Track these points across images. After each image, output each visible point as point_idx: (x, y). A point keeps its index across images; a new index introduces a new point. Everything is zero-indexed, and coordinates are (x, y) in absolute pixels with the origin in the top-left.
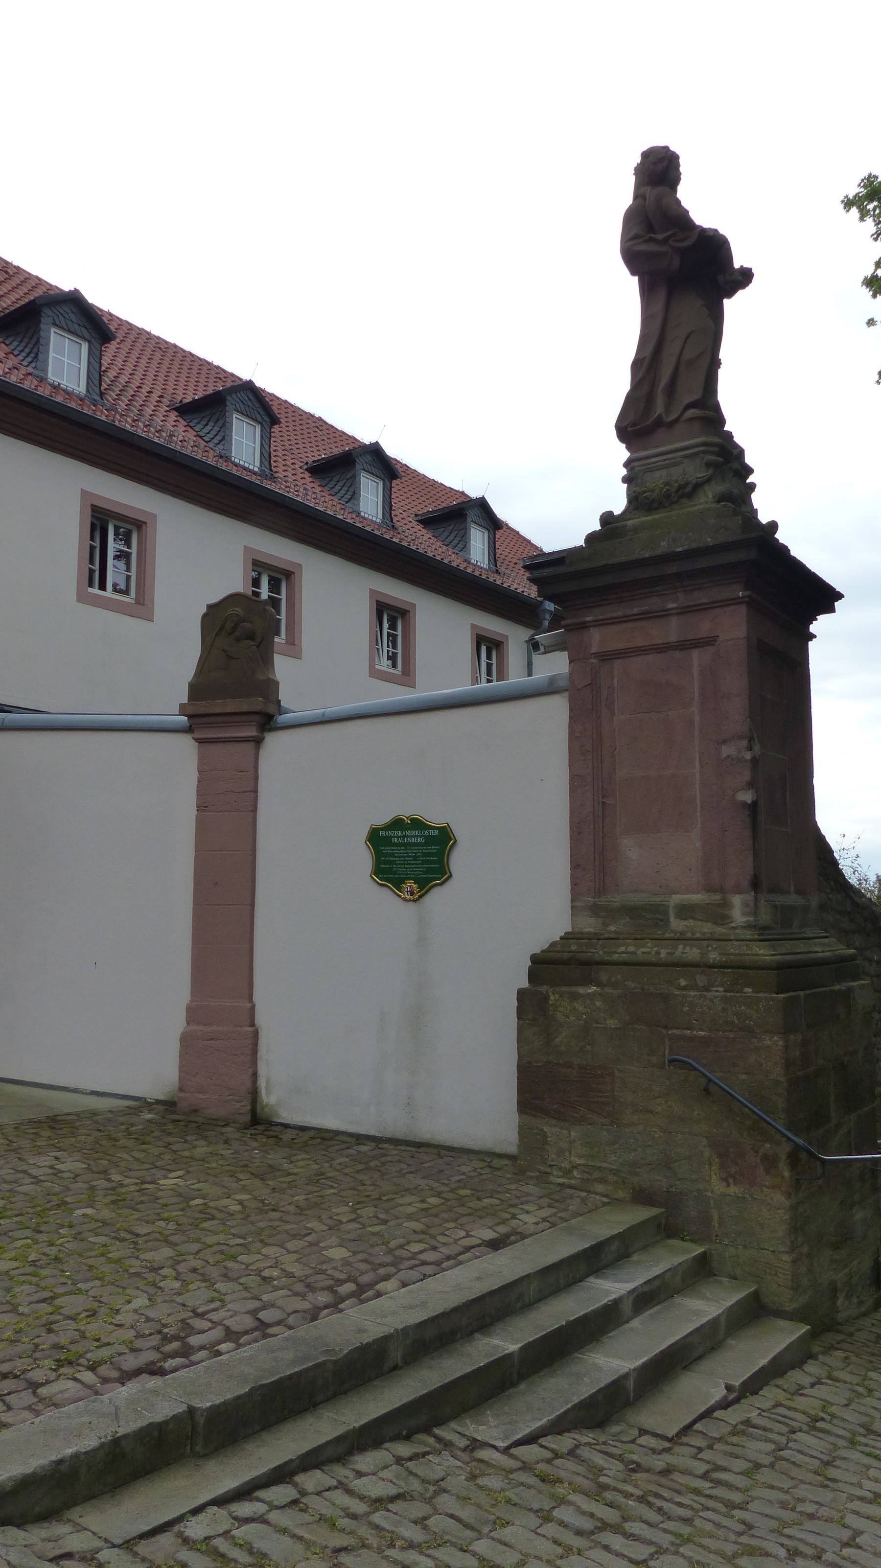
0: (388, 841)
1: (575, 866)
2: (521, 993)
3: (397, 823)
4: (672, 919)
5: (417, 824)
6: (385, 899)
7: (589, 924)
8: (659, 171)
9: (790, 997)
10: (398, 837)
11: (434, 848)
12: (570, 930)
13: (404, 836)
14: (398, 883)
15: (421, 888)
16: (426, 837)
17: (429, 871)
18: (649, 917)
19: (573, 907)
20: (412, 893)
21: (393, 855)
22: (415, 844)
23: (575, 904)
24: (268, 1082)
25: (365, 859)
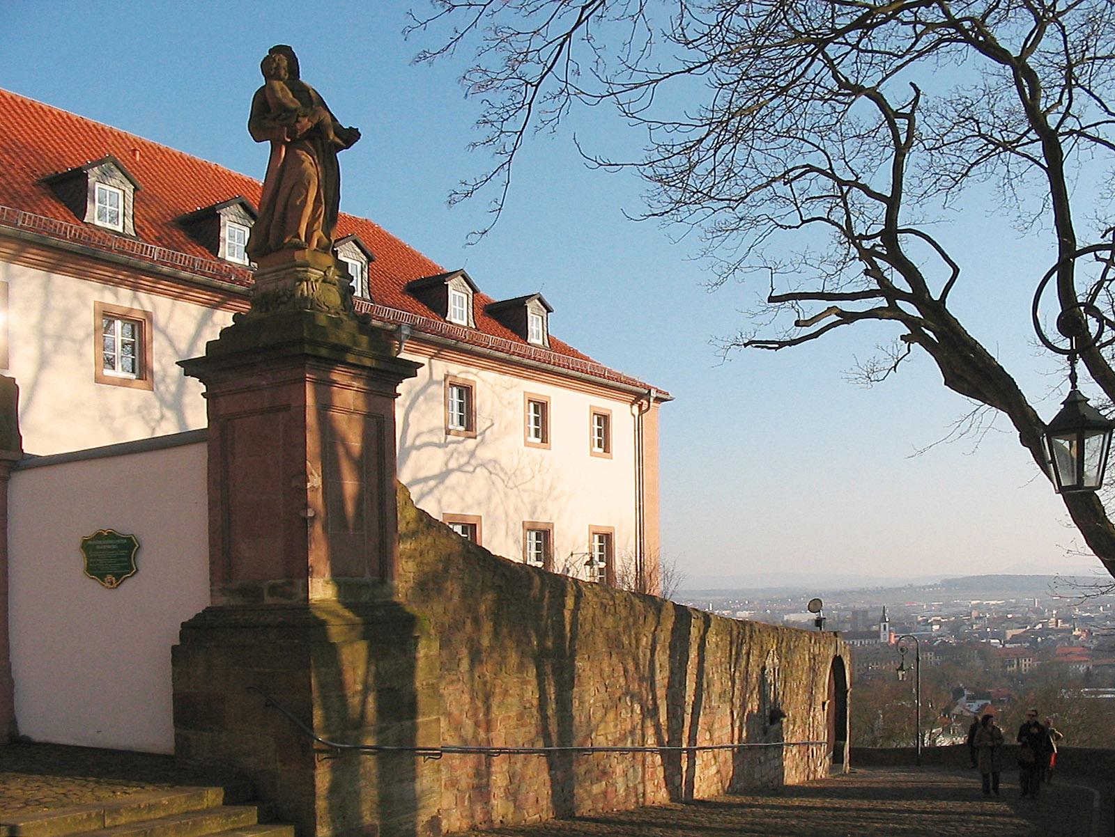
0: (94, 548)
1: (212, 563)
2: (174, 648)
3: (99, 536)
4: (266, 597)
5: (112, 535)
6: (93, 586)
7: (222, 601)
8: (281, 63)
9: (564, 627)
10: (100, 545)
11: (124, 553)
12: (209, 605)
13: (836, 825)
14: (102, 577)
15: (117, 580)
16: (118, 545)
17: (123, 568)
18: (251, 592)
19: (211, 590)
20: (112, 584)
21: (97, 557)
22: (111, 550)
23: (214, 588)
24: (1073, 476)
25: (80, 561)
